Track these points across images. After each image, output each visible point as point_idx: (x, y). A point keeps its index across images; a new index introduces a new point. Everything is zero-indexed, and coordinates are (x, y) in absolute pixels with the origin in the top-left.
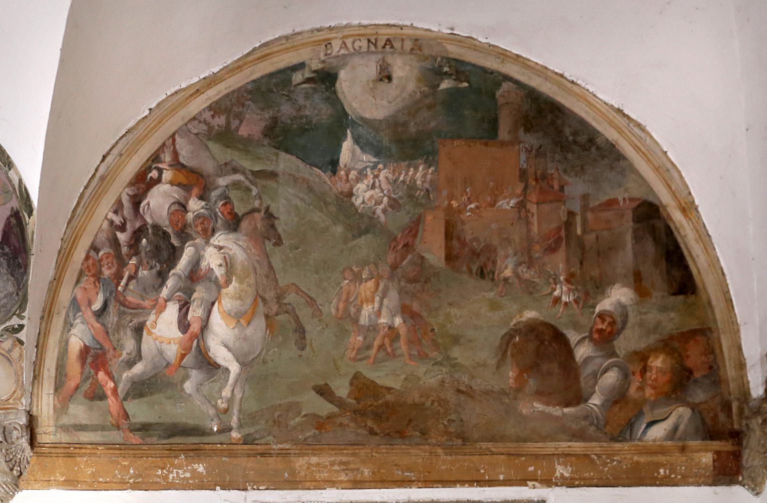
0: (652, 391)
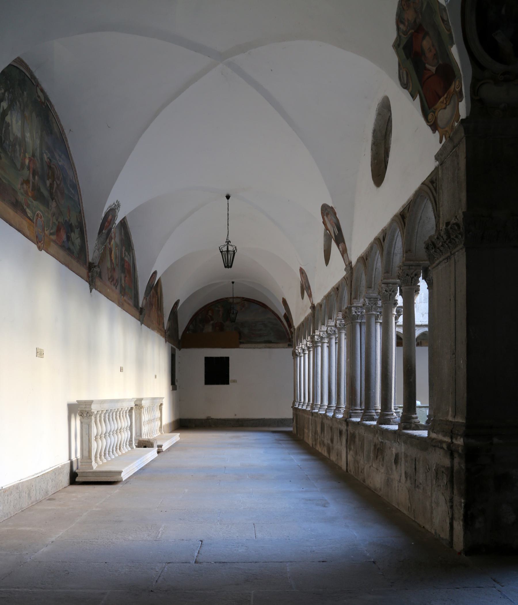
0: (441, 244)
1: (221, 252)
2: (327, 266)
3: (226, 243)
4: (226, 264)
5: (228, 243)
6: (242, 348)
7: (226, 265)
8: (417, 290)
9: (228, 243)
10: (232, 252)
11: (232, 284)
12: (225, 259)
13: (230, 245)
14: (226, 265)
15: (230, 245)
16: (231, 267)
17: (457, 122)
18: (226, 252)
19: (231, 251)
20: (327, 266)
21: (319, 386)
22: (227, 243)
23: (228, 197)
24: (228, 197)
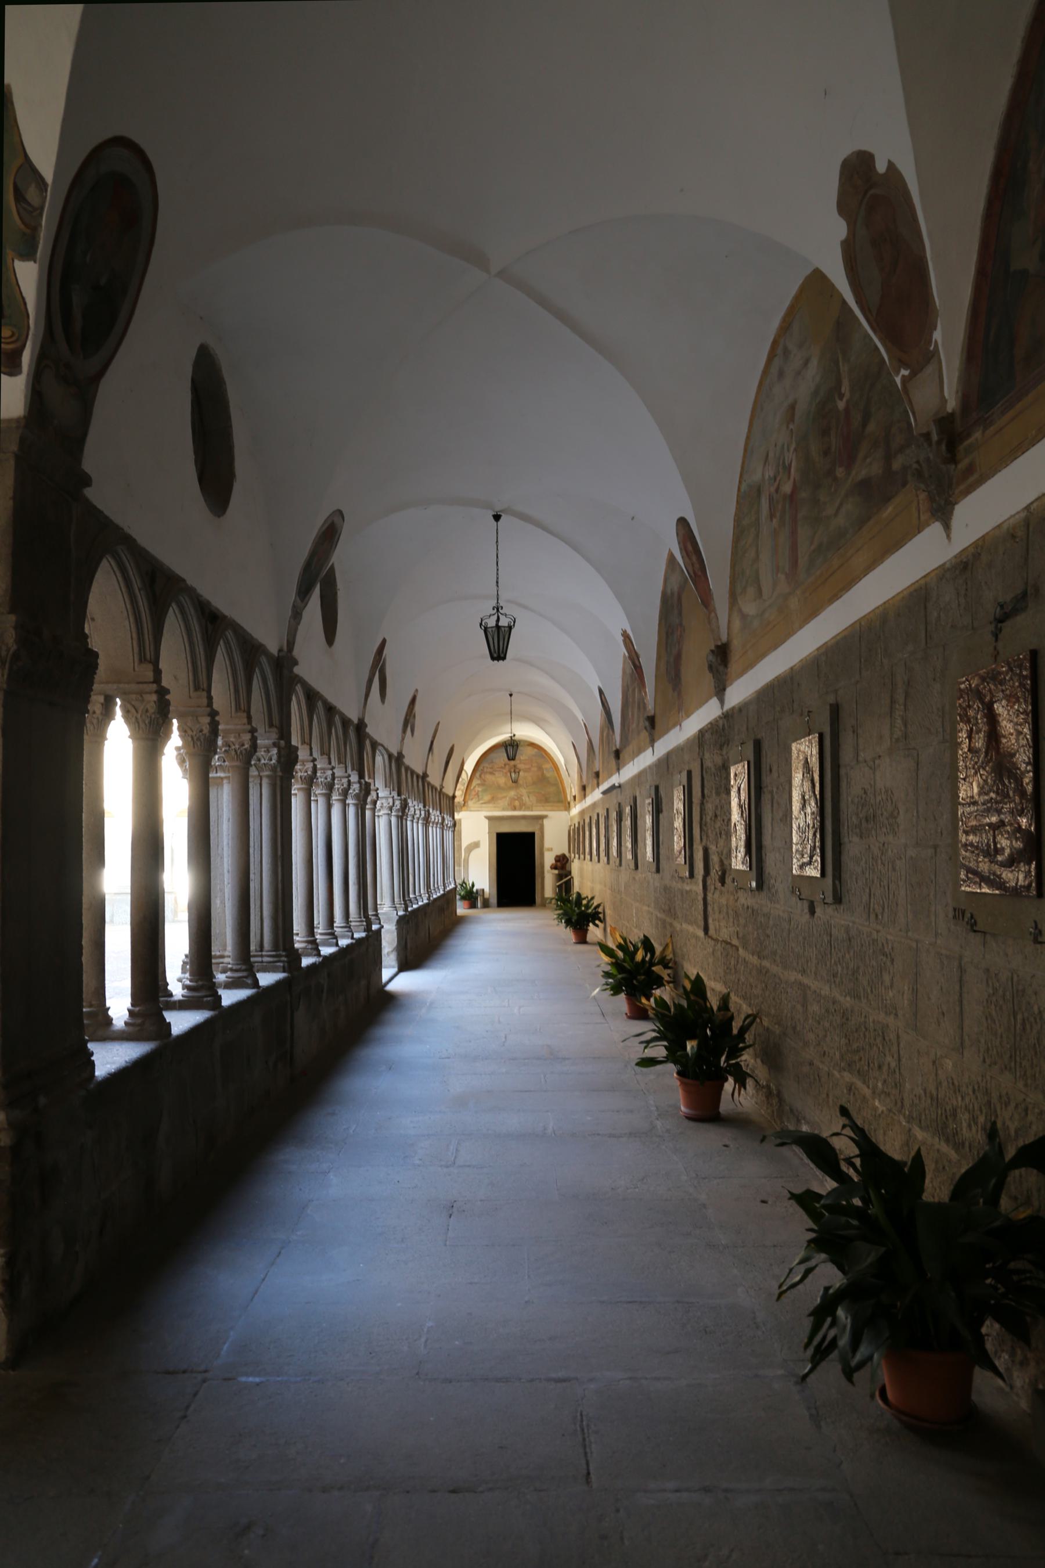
1: (486, 630)
2: (889, 161)
3: (493, 609)
4: (495, 652)
5: (498, 610)
6: (1018, 513)
7: (495, 655)
8: (167, 735)
9: (498, 610)
10: (507, 629)
11: (496, 523)
12: (494, 646)
13: (501, 614)
14: (495, 655)
15: (501, 614)
16: (504, 658)
17: (28, 255)
18: (494, 629)
19: (504, 627)
20: (889, 161)
21: (321, 865)
22: (496, 609)
23: (511, 695)
24: (511, 695)
